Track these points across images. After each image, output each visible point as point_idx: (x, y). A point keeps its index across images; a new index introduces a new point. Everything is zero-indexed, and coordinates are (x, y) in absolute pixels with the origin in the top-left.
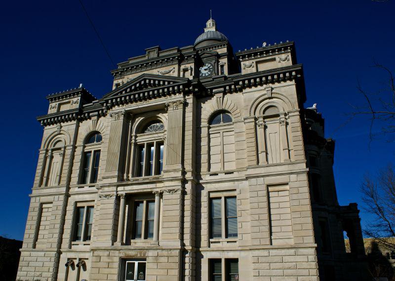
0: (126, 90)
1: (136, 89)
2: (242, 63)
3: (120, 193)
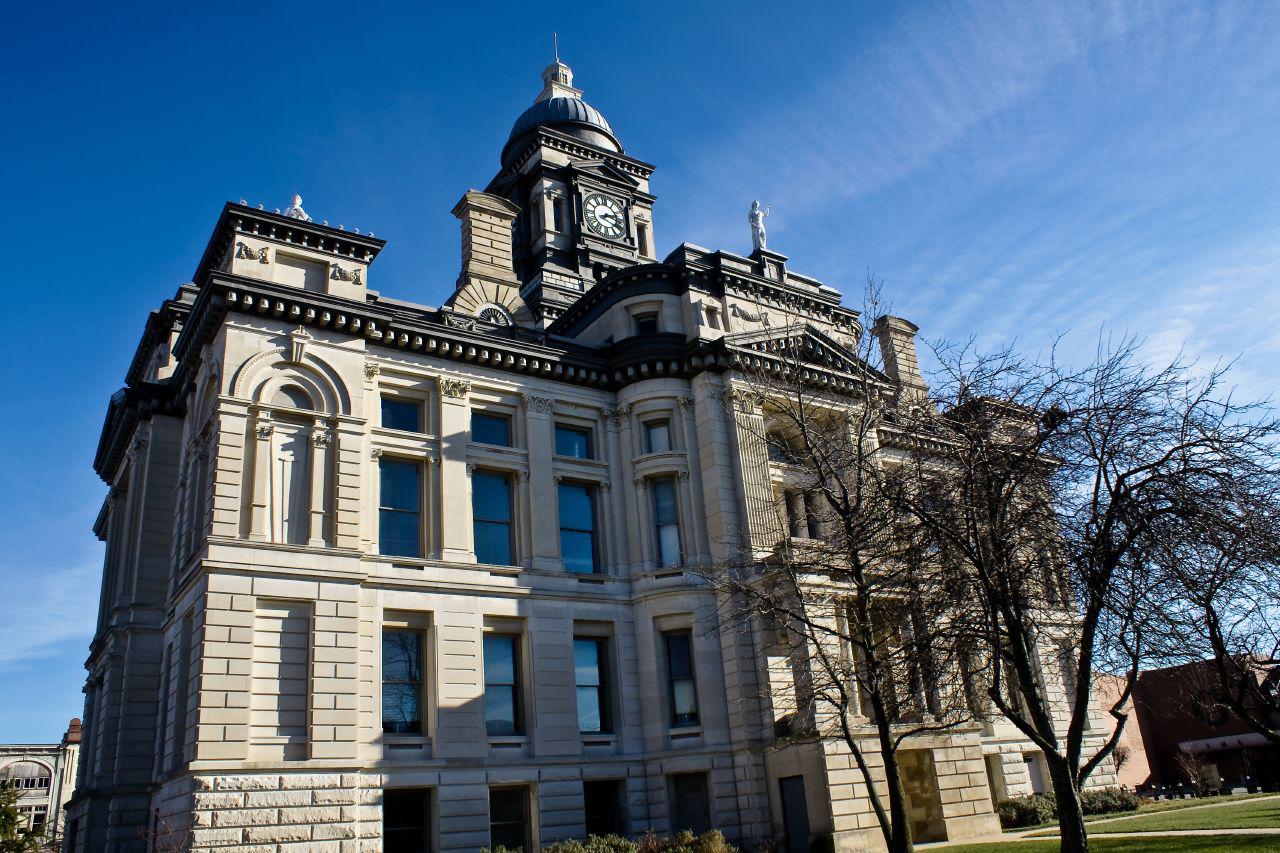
2: (239, 238)
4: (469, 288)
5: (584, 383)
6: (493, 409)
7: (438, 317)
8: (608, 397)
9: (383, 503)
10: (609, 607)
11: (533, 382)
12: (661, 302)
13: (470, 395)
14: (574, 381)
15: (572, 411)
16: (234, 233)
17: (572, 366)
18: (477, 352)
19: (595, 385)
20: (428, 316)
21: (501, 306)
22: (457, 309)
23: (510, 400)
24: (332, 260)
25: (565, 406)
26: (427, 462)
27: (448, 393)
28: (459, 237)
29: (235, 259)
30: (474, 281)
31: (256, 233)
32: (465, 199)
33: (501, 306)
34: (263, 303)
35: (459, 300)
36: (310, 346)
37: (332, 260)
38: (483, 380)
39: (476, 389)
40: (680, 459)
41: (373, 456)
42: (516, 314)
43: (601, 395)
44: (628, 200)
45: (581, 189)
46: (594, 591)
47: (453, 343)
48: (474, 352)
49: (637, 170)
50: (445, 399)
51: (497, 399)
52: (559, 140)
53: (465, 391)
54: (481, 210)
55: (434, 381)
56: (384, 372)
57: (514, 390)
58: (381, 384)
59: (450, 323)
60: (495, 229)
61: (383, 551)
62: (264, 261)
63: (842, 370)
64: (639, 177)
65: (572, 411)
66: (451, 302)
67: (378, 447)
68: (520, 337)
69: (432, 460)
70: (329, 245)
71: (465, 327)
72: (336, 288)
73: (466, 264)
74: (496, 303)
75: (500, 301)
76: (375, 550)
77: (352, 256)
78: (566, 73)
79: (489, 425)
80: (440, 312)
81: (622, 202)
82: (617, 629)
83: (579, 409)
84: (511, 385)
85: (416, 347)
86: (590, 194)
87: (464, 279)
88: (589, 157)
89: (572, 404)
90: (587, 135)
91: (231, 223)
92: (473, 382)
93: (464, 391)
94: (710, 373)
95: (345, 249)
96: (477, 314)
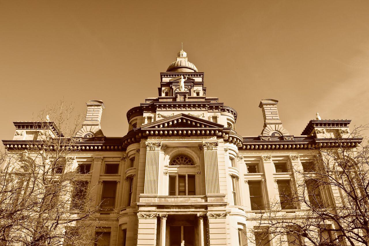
0: (159, 126)
1: (168, 126)
2: (316, 129)
3: (161, 214)
4: (266, 128)
5: (114, 150)
6: (85, 163)
7: (258, 139)
8: (123, 153)
9: (251, 195)
10: (110, 223)
11: (97, 153)
12: (137, 119)
13: (272, 159)
14: (110, 150)
15: (111, 160)
16: (314, 128)
17: (16, 144)
18: (295, 146)
19: (118, 150)
20: (255, 139)
21: (277, 131)
22: (264, 135)
23: (89, 160)
24: (339, 128)
25: (109, 158)
26: (290, 180)
27: (265, 160)
28: (262, 113)
29: (317, 134)
30: (268, 125)
31: (21, 128)
32: (261, 103)
33: (277, 131)
34: (349, 144)
35: (264, 132)
36: (26, 153)
37: (339, 128)
38: (282, 154)
39: (245, 157)
40: (134, 170)
41: (275, 181)
42: (95, 134)
43: (121, 153)
44: (191, 86)
45: (173, 87)
46: (105, 217)
47: (288, 145)
48: (294, 146)
49: (192, 75)
50: (264, 162)
51: (253, 159)
52: (198, 74)
53: (270, 158)
54: (267, 104)
55: (260, 157)
56: (245, 157)
57: (90, 156)
58: (273, 160)
59: (285, 139)
60: (272, 109)
61: (253, 209)
62: (323, 133)
63: (201, 126)
64: (193, 77)
65: (111, 160)
66: (262, 133)
67: (247, 179)
68: (96, 140)
69: (292, 179)
70: (337, 124)
71: (290, 139)
72: (344, 136)
73: (265, 121)
74: (276, 130)
75: (277, 129)
76: (250, 209)
77: (319, 126)
78: (185, 54)
79: (84, 168)
80: (259, 137)
81: (189, 87)
82: (112, 230)
83: (114, 158)
84: (89, 155)
85: (286, 148)
86: (176, 88)
87: (265, 126)
88: (177, 76)
89: (112, 157)
90: (180, 70)
91: (312, 125)
92: (272, 155)
93: (269, 158)
94: (143, 139)
95: (341, 124)
96: (270, 135)
